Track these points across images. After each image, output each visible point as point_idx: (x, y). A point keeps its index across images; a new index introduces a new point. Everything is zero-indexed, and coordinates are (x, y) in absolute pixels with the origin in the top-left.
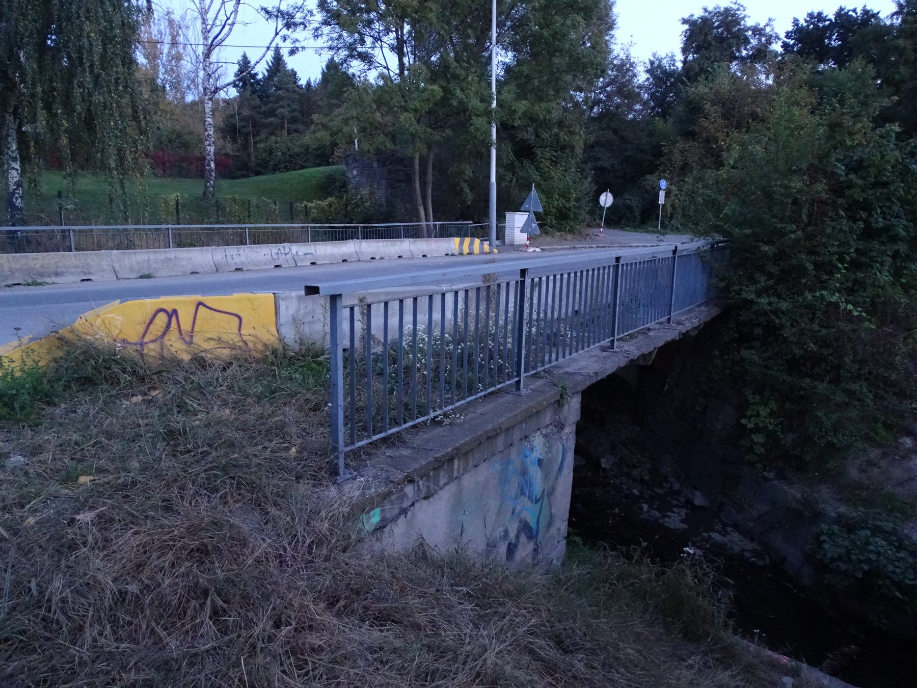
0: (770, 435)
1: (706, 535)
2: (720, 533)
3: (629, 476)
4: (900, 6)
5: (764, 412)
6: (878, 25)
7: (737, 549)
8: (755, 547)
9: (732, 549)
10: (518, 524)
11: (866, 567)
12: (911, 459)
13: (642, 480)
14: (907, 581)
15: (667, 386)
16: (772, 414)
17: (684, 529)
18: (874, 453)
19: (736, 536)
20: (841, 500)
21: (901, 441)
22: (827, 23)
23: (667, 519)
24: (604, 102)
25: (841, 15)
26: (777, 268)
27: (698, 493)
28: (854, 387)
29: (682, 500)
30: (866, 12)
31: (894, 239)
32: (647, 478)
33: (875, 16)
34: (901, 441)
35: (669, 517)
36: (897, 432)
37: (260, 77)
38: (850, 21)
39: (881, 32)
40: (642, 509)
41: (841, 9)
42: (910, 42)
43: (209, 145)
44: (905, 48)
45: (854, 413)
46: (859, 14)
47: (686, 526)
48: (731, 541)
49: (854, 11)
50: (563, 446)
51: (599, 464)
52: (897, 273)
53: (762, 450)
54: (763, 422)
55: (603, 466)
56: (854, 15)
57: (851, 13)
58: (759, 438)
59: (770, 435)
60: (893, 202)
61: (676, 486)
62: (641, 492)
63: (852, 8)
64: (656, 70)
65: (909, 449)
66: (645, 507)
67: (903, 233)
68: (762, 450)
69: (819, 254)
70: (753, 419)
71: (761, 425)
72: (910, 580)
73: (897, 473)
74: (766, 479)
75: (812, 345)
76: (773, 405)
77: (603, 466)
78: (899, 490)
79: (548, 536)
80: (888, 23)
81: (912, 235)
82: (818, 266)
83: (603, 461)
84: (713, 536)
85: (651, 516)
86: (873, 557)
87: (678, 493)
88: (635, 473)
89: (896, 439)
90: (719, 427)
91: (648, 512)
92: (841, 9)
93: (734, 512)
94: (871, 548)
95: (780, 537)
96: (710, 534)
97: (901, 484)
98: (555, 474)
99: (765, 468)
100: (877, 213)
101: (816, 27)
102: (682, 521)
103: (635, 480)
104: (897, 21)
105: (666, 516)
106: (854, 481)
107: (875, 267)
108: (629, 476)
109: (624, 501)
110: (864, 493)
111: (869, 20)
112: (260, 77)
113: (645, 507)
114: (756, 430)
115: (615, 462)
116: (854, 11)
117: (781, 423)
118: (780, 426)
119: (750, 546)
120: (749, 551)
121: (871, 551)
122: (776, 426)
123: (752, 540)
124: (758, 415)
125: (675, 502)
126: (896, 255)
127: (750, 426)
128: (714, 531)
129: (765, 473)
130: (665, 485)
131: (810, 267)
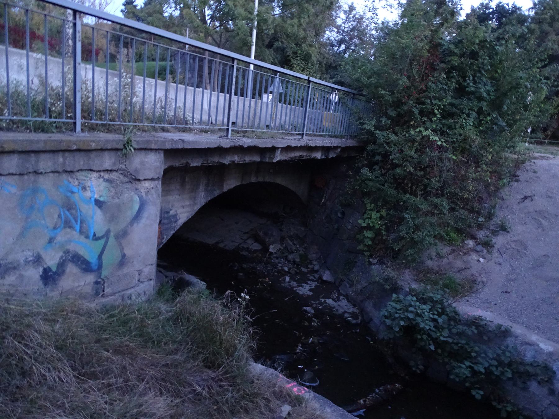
0: (378, 233)
1: (323, 300)
2: (334, 300)
3: (286, 258)
4: (535, 4)
5: (375, 215)
6: (521, 14)
7: (341, 311)
8: (355, 311)
9: (337, 310)
10: (61, 254)
11: (402, 323)
12: (470, 255)
13: (294, 262)
14: (442, 338)
15: (323, 200)
16: (381, 218)
17: (308, 295)
18: (446, 249)
19: (344, 302)
20: (416, 280)
21: (466, 242)
22: (491, 10)
23: (301, 288)
24: (347, 42)
25: (500, 7)
26: (395, 112)
27: (327, 272)
28: (437, 201)
29: (317, 276)
30: (515, 7)
31: (480, 99)
32: (298, 260)
33: (520, 9)
34: (466, 242)
35: (302, 287)
36: (465, 236)
37: (138, 8)
38: (505, 10)
39: (522, 19)
40: (284, 280)
41: (500, 3)
42: (537, 26)
43: (69, 28)
44: (534, 30)
45: (434, 220)
46: (510, 7)
47: (311, 293)
48: (339, 305)
49: (508, 5)
50: (141, 198)
51: (268, 249)
52: (478, 124)
53: (370, 243)
54: (373, 222)
55: (270, 250)
56: (507, 7)
57: (505, 5)
58: (369, 234)
59: (378, 233)
60: (482, 74)
61: (316, 268)
62: (289, 269)
63: (507, 3)
64: (385, 29)
65: (470, 248)
66: (287, 279)
67: (485, 95)
68: (370, 243)
69: (423, 103)
70: (367, 221)
71: (371, 225)
72: (444, 337)
73: (459, 264)
74: (371, 264)
75: (411, 168)
76: (384, 213)
77: (270, 250)
78: (458, 275)
79: (120, 273)
80: (527, 13)
81: (492, 97)
82: (421, 113)
83: (271, 247)
84: (327, 301)
85: (290, 285)
86: (411, 316)
87: (316, 271)
88: (290, 257)
89: (463, 241)
90: (349, 227)
91: (289, 282)
92: (500, 3)
93: (348, 286)
94: (411, 309)
95: (372, 304)
96: (327, 300)
97: (460, 271)
98: (129, 219)
99: (371, 256)
100: (469, 80)
101: (484, 13)
102: (310, 290)
103: (289, 261)
104: (532, 13)
105: (299, 286)
106: (428, 268)
107: (462, 117)
108: (286, 258)
109: (276, 274)
110: (433, 276)
111: (515, 11)
112: (138, 8)
113: (287, 279)
114: (368, 228)
115: (280, 249)
116: (508, 5)
117: (386, 224)
118: (384, 227)
119: (351, 309)
120: (349, 313)
121: (412, 312)
122: (382, 226)
123: (354, 305)
124: (371, 218)
125: (312, 278)
126: (480, 112)
127: (364, 225)
128: (329, 298)
129: (371, 260)
130: (309, 266)
131: (416, 111)
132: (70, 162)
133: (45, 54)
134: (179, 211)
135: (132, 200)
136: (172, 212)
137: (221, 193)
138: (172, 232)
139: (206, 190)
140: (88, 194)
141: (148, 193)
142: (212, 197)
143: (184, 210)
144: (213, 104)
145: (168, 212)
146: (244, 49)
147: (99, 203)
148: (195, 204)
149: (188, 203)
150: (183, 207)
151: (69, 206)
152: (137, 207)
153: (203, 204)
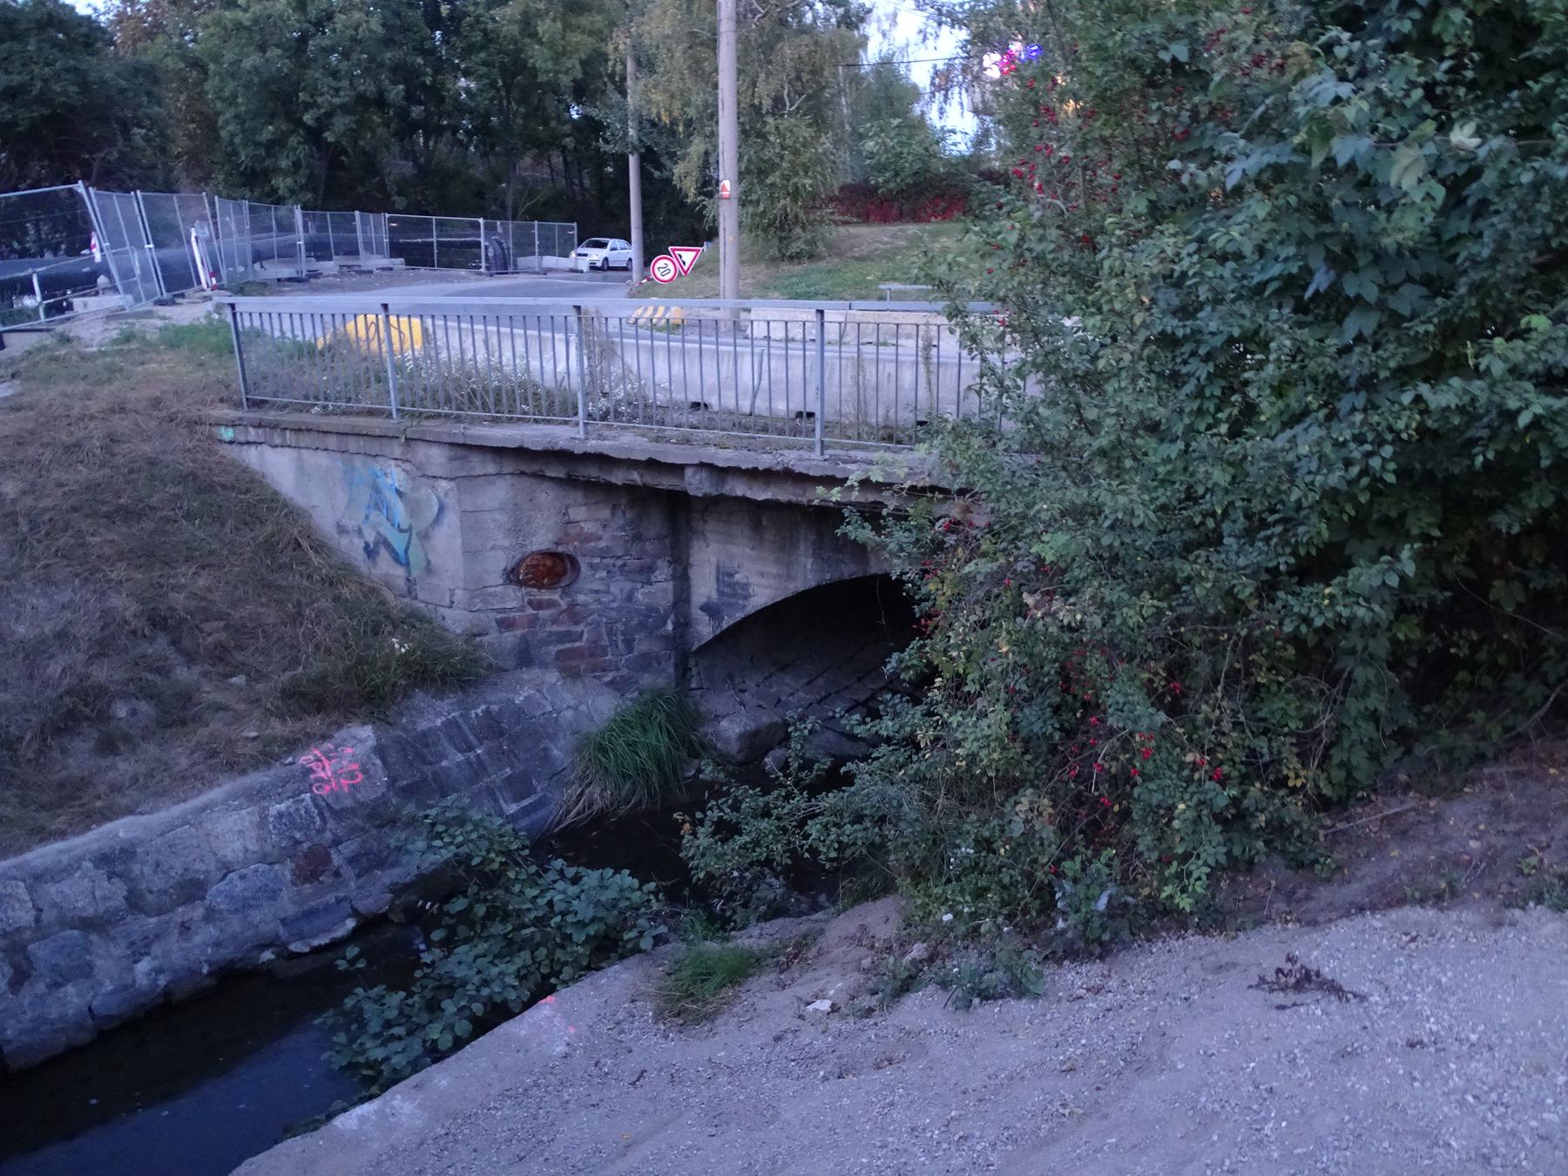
132: (375, 447)
133: (735, 195)
134: (754, 580)
135: (429, 499)
136: (737, 577)
137: (860, 575)
138: (739, 616)
139: (816, 555)
140: (389, 481)
141: (446, 494)
142: (837, 576)
143: (764, 582)
144: (548, 355)
145: (731, 575)
146: (440, 244)
147: (399, 493)
148: (789, 577)
149: (773, 570)
150: (762, 575)
151: (377, 489)
152: (436, 509)
153: (813, 584)
